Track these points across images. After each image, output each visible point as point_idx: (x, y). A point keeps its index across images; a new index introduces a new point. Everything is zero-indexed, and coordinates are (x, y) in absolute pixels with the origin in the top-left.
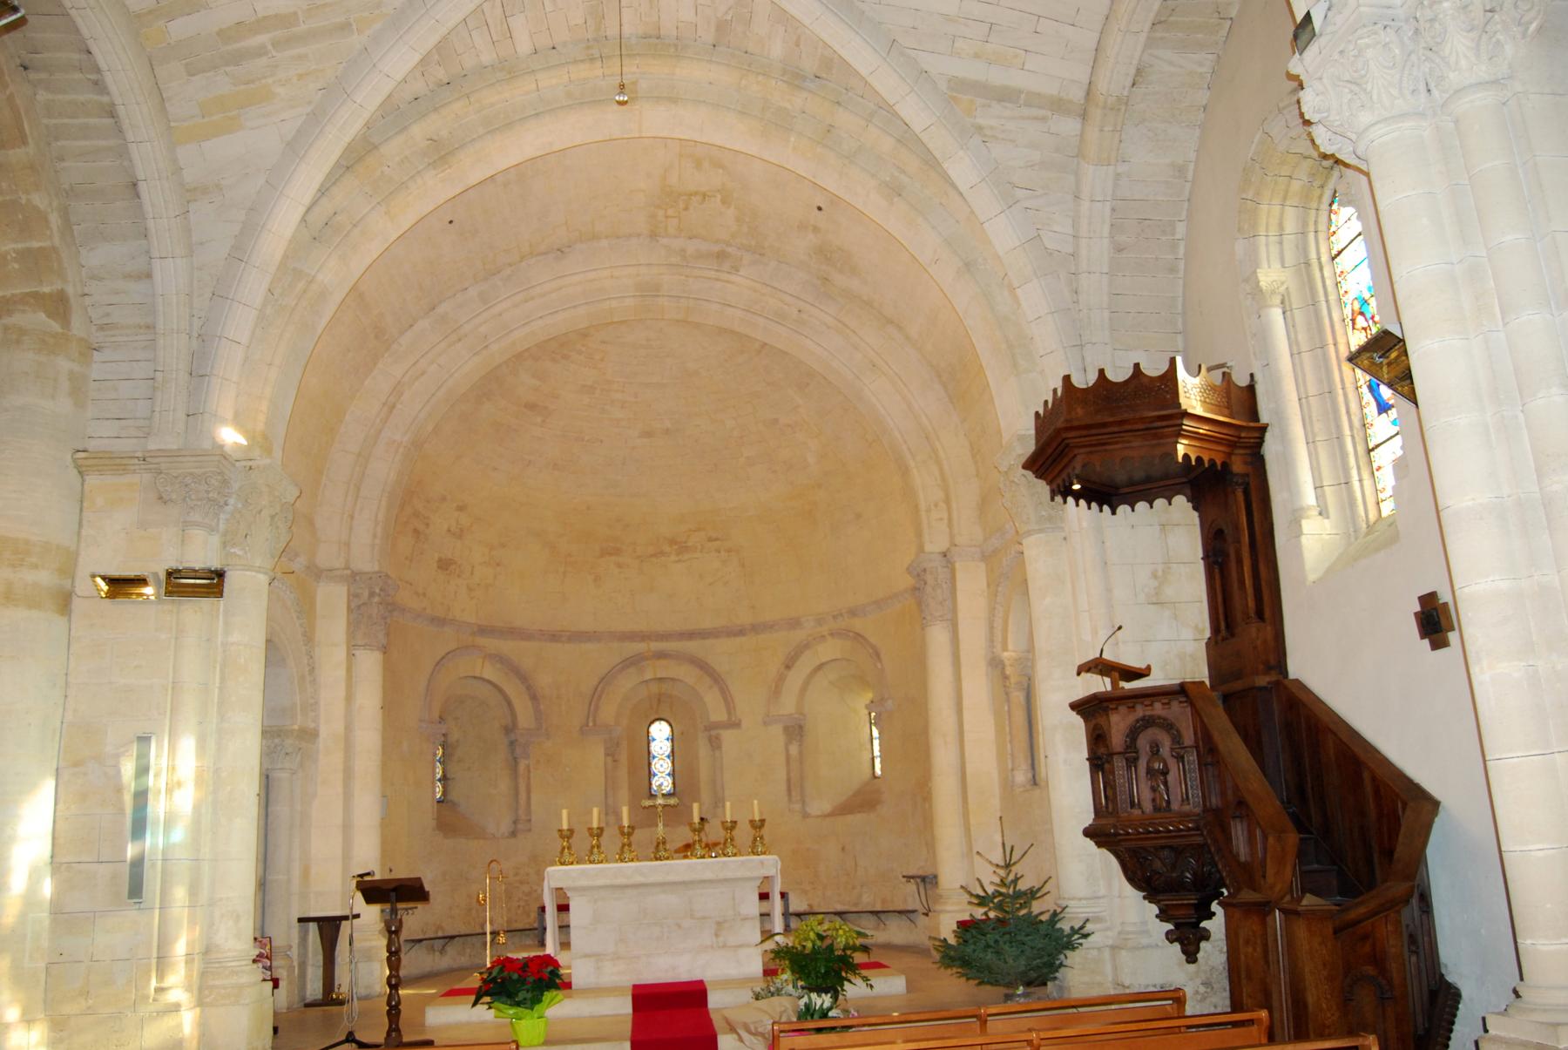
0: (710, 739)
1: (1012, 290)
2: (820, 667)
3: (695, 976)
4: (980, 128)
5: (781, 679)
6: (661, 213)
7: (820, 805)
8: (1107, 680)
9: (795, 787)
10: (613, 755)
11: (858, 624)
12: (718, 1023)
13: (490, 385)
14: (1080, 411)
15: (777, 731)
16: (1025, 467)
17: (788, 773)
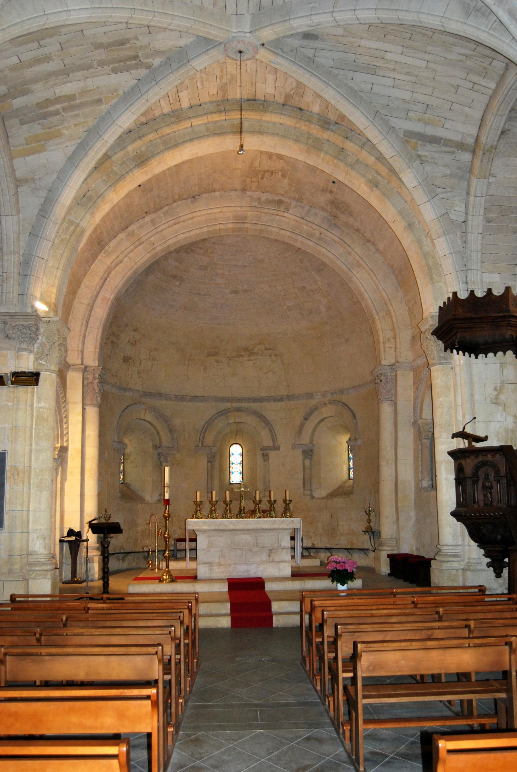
0: (263, 455)
1: (432, 240)
2: (322, 420)
3: (259, 575)
4: (419, 156)
5: (302, 426)
6: (248, 180)
7: (321, 493)
8: (466, 441)
9: (308, 482)
10: (211, 462)
11: (344, 398)
12: (270, 597)
13: (153, 267)
14: (460, 310)
15: (299, 452)
16: (433, 334)
17: (304, 475)
